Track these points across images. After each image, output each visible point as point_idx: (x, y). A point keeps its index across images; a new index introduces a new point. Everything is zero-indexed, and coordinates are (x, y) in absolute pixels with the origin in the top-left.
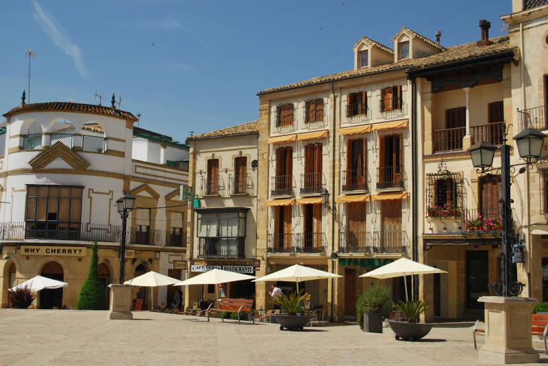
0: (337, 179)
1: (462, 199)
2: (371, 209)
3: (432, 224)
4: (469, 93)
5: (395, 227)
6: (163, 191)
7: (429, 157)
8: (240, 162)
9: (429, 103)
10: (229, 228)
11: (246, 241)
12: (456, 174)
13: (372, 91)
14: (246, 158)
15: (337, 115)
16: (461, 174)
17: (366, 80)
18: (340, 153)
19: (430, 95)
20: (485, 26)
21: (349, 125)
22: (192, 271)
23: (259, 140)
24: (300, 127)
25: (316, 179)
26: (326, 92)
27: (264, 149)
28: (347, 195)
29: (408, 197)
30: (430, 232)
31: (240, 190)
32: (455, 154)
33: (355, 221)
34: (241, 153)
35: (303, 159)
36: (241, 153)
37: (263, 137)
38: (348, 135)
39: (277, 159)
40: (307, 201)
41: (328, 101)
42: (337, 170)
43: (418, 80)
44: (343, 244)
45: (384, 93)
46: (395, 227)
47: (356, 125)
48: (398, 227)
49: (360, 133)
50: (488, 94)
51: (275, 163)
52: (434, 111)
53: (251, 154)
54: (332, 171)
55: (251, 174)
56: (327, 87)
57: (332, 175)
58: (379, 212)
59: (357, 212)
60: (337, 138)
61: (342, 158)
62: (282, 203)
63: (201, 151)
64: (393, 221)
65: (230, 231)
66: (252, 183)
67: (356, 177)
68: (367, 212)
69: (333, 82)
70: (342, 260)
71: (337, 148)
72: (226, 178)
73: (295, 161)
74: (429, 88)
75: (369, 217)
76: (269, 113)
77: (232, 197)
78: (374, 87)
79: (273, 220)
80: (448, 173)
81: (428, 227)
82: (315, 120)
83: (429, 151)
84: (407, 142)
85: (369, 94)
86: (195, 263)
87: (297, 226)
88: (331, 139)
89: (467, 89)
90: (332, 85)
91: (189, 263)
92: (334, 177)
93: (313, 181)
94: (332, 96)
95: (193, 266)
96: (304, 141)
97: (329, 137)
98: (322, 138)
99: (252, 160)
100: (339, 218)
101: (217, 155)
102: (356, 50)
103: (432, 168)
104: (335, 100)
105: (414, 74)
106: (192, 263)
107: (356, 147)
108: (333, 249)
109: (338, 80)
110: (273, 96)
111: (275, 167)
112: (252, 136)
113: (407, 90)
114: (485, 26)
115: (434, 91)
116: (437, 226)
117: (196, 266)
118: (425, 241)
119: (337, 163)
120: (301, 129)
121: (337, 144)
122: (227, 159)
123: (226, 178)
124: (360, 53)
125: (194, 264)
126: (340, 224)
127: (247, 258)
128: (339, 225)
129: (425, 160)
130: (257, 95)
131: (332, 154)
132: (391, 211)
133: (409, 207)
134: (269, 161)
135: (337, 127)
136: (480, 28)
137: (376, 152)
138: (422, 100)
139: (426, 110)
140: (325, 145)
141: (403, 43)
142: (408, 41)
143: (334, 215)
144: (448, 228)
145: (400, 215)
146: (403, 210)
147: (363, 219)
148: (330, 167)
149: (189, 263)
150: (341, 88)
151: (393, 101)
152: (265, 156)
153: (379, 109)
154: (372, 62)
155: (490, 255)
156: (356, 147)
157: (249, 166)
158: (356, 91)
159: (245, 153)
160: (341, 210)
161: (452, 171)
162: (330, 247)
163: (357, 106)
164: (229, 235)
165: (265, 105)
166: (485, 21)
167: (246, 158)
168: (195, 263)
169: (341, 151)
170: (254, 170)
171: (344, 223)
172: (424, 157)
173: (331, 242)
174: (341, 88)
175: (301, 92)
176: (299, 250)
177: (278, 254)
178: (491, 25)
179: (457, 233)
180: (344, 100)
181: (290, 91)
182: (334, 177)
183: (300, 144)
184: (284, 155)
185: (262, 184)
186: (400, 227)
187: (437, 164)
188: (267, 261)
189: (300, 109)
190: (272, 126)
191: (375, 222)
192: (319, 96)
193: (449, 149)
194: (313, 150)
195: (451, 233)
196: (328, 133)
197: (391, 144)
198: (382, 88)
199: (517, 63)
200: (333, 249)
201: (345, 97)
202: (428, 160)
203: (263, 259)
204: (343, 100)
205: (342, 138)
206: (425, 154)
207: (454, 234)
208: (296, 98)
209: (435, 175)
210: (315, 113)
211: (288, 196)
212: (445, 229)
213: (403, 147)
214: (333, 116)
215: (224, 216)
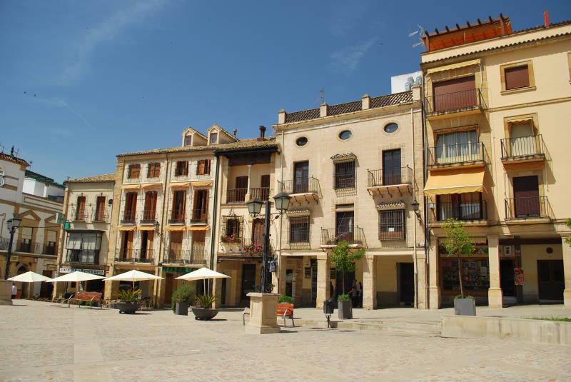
8: (101, 200)
53: (109, 195)
59: (177, 237)
67: (177, 215)
70: (165, 268)
89: (249, 166)
90: (167, 155)
105: (218, 154)
118: (219, 257)
120: (144, 181)
122: (91, 197)
123: (90, 210)
157: (107, 203)
163: (182, 169)
185: (115, 215)
199: (279, 153)
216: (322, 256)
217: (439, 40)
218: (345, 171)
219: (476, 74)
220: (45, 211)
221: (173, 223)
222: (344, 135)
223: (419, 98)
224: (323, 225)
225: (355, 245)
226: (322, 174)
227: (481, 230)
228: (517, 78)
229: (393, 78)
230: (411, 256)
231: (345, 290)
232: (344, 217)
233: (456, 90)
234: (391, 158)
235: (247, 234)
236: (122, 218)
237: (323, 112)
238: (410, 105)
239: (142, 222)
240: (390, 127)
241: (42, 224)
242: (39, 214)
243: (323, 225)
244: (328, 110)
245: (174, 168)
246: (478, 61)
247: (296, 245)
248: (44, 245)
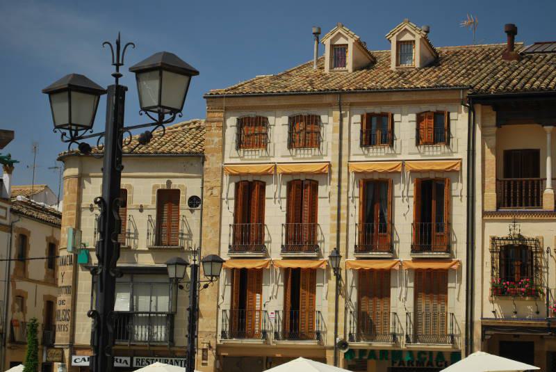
0: (343, 234)
1: (541, 274)
2: (401, 280)
3: (496, 305)
4: (552, 134)
5: (435, 308)
7: (491, 213)
8: (167, 198)
9: (493, 141)
10: (154, 298)
11: (176, 318)
12: (533, 240)
13: (402, 114)
14: (178, 191)
15: (345, 142)
16: (541, 240)
17: (395, 98)
18: (348, 198)
19: (494, 130)
20: (512, 32)
21: (363, 158)
22: (73, 364)
23: (206, 166)
24: (278, 154)
25: (254, 234)
26: (330, 106)
27: (211, 180)
28: (358, 258)
29: (460, 267)
30: (492, 316)
31: (165, 240)
32: (532, 213)
33: (370, 297)
34: (169, 183)
35: (284, 202)
36: (169, 183)
37: (212, 163)
38: (364, 173)
39: (288, 197)
40: (239, 265)
41: (329, 124)
42: (343, 222)
43: (478, 108)
44: (352, 328)
45: (419, 119)
46: (435, 308)
47: (377, 159)
48: (439, 307)
49: (386, 173)
51: (232, 203)
52: (496, 151)
53: (189, 186)
54: (336, 222)
55: (189, 220)
56: (329, 99)
57: (336, 229)
58: (412, 284)
59: (375, 286)
60: (344, 175)
61: (352, 205)
62: (249, 265)
63: (91, 174)
64: (432, 299)
65: (153, 304)
66: (189, 231)
68: (392, 284)
70: (351, 352)
71: (344, 189)
73: (269, 204)
74: (492, 120)
75: (394, 293)
76: (224, 128)
77: (151, 250)
78: (405, 108)
79: (229, 289)
80: (521, 238)
81: (488, 308)
82: (304, 146)
83: (491, 205)
84: (459, 189)
85: (397, 117)
86: (78, 352)
87: (271, 301)
88: (335, 176)
91: (67, 352)
92: (338, 231)
93: (301, 232)
94: (337, 113)
95: (74, 358)
96: (284, 174)
97: (330, 172)
98: (320, 173)
99: (189, 195)
100: (346, 290)
102: (327, 42)
103: (501, 229)
104: (341, 120)
105: (476, 100)
106: (73, 353)
107: (376, 192)
108: (336, 336)
109: (349, 92)
110: (233, 103)
111: (232, 210)
113: (459, 122)
114: (512, 32)
115: (498, 125)
116: (503, 308)
117: (81, 357)
119: (343, 211)
121: (344, 184)
125: (75, 354)
126: (348, 299)
127: (177, 345)
128: (346, 302)
129: (486, 218)
130: (204, 97)
131: (335, 197)
132: (431, 285)
133: (460, 281)
134: (221, 199)
135: (345, 160)
136: (506, 34)
137: (407, 200)
138: (483, 135)
139: (487, 150)
140: (322, 185)
141: (404, 42)
142: (414, 41)
143: (338, 286)
144: (519, 313)
145: (389, 296)
146: (449, 285)
147: (385, 294)
148: (332, 216)
149: (67, 352)
150: (351, 104)
151: (435, 131)
152: (216, 192)
154: (355, 62)
155: (537, 348)
156: (250, 193)
159: (176, 184)
160: (350, 279)
161: (526, 235)
162: (331, 333)
163: (377, 132)
164: (153, 310)
165: (216, 114)
166: (514, 25)
167: (178, 191)
168: (78, 352)
169: (350, 195)
170: (192, 211)
171: (354, 298)
172: (484, 213)
173: (333, 324)
174: (351, 104)
175: (283, 102)
177: (235, 341)
178: (519, 31)
179: (533, 320)
180: (355, 124)
181: (263, 98)
182: (338, 231)
183: (280, 178)
186: (443, 309)
187: (508, 224)
188: (217, 350)
189: (279, 128)
190: (227, 147)
191: (405, 298)
192: (313, 111)
193: (521, 205)
194: (302, 191)
195: (526, 319)
196: (330, 166)
197: (432, 193)
198: (419, 111)
200: (336, 336)
201: (357, 118)
202: (489, 218)
203: (210, 347)
204: (353, 121)
205: (352, 176)
206: (486, 209)
207: (530, 319)
208: (274, 109)
209: (502, 239)
210: (305, 133)
211: (386, 254)
212: (516, 313)
213: (450, 196)
214: (337, 142)
215: (138, 278)
221: (293, 251)
229: (121, 188)
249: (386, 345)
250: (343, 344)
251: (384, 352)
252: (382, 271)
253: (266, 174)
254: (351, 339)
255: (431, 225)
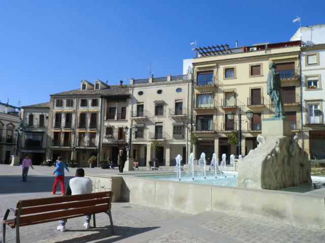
6: (6, 123)
8: (42, 117)
47: (82, 109)
50: (122, 105)
53: (46, 114)
59: (82, 135)
62: (82, 131)
67: (58, 124)
69: (77, 95)
70: (76, 149)
72: (36, 122)
74: (106, 101)
89: (117, 103)
90: (76, 96)
101: (33, 113)
105: (102, 97)
112: (47, 109)
118: (103, 144)
120: (66, 109)
122: (37, 116)
123: (36, 122)
124: (83, 85)
153: (321, 91)
156: (58, 116)
157: (45, 118)
158: (95, 99)
159: (44, 114)
163: (84, 103)
176: (62, 146)
184: (58, 116)
185: (50, 125)
194: (69, 116)
199: (130, 98)
216: (149, 144)
217: (205, 52)
218: (159, 108)
219: (214, 69)
220: (6, 120)
221: (92, 128)
222: (160, 92)
223: (191, 78)
224: (150, 130)
225: (163, 140)
226: (149, 109)
227: (212, 135)
228: (229, 72)
229: (184, 60)
230: (185, 145)
231: (159, 160)
232: (159, 129)
233: (204, 77)
234: (178, 105)
235: (116, 134)
236: (54, 126)
237: (150, 81)
238: (187, 81)
239: (65, 128)
240: (179, 90)
241: (5, 127)
242: (14, 124)
243: (150, 130)
244: (153, 80)
245: (80, 102)
246: (215, 65)
247: (138, 139)
248: (7, 138)
249: (83, 148)
250: (74, 148)
251: (83, 149)
252: (94, 133)
253: (61, 112)
254: (76, 146)
255: (94, 123)
